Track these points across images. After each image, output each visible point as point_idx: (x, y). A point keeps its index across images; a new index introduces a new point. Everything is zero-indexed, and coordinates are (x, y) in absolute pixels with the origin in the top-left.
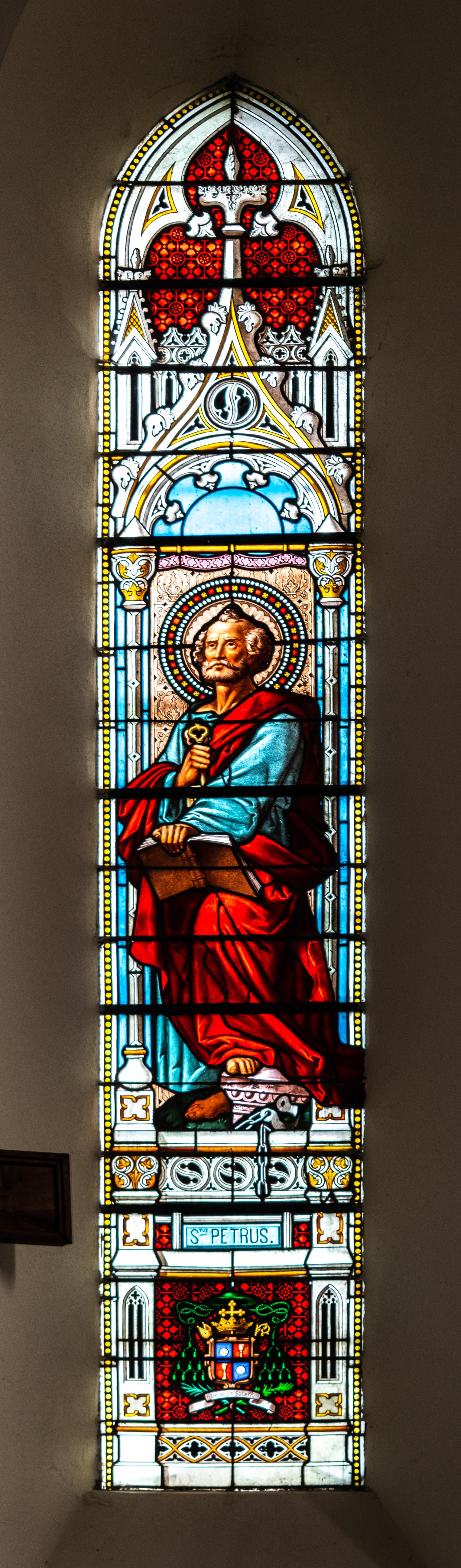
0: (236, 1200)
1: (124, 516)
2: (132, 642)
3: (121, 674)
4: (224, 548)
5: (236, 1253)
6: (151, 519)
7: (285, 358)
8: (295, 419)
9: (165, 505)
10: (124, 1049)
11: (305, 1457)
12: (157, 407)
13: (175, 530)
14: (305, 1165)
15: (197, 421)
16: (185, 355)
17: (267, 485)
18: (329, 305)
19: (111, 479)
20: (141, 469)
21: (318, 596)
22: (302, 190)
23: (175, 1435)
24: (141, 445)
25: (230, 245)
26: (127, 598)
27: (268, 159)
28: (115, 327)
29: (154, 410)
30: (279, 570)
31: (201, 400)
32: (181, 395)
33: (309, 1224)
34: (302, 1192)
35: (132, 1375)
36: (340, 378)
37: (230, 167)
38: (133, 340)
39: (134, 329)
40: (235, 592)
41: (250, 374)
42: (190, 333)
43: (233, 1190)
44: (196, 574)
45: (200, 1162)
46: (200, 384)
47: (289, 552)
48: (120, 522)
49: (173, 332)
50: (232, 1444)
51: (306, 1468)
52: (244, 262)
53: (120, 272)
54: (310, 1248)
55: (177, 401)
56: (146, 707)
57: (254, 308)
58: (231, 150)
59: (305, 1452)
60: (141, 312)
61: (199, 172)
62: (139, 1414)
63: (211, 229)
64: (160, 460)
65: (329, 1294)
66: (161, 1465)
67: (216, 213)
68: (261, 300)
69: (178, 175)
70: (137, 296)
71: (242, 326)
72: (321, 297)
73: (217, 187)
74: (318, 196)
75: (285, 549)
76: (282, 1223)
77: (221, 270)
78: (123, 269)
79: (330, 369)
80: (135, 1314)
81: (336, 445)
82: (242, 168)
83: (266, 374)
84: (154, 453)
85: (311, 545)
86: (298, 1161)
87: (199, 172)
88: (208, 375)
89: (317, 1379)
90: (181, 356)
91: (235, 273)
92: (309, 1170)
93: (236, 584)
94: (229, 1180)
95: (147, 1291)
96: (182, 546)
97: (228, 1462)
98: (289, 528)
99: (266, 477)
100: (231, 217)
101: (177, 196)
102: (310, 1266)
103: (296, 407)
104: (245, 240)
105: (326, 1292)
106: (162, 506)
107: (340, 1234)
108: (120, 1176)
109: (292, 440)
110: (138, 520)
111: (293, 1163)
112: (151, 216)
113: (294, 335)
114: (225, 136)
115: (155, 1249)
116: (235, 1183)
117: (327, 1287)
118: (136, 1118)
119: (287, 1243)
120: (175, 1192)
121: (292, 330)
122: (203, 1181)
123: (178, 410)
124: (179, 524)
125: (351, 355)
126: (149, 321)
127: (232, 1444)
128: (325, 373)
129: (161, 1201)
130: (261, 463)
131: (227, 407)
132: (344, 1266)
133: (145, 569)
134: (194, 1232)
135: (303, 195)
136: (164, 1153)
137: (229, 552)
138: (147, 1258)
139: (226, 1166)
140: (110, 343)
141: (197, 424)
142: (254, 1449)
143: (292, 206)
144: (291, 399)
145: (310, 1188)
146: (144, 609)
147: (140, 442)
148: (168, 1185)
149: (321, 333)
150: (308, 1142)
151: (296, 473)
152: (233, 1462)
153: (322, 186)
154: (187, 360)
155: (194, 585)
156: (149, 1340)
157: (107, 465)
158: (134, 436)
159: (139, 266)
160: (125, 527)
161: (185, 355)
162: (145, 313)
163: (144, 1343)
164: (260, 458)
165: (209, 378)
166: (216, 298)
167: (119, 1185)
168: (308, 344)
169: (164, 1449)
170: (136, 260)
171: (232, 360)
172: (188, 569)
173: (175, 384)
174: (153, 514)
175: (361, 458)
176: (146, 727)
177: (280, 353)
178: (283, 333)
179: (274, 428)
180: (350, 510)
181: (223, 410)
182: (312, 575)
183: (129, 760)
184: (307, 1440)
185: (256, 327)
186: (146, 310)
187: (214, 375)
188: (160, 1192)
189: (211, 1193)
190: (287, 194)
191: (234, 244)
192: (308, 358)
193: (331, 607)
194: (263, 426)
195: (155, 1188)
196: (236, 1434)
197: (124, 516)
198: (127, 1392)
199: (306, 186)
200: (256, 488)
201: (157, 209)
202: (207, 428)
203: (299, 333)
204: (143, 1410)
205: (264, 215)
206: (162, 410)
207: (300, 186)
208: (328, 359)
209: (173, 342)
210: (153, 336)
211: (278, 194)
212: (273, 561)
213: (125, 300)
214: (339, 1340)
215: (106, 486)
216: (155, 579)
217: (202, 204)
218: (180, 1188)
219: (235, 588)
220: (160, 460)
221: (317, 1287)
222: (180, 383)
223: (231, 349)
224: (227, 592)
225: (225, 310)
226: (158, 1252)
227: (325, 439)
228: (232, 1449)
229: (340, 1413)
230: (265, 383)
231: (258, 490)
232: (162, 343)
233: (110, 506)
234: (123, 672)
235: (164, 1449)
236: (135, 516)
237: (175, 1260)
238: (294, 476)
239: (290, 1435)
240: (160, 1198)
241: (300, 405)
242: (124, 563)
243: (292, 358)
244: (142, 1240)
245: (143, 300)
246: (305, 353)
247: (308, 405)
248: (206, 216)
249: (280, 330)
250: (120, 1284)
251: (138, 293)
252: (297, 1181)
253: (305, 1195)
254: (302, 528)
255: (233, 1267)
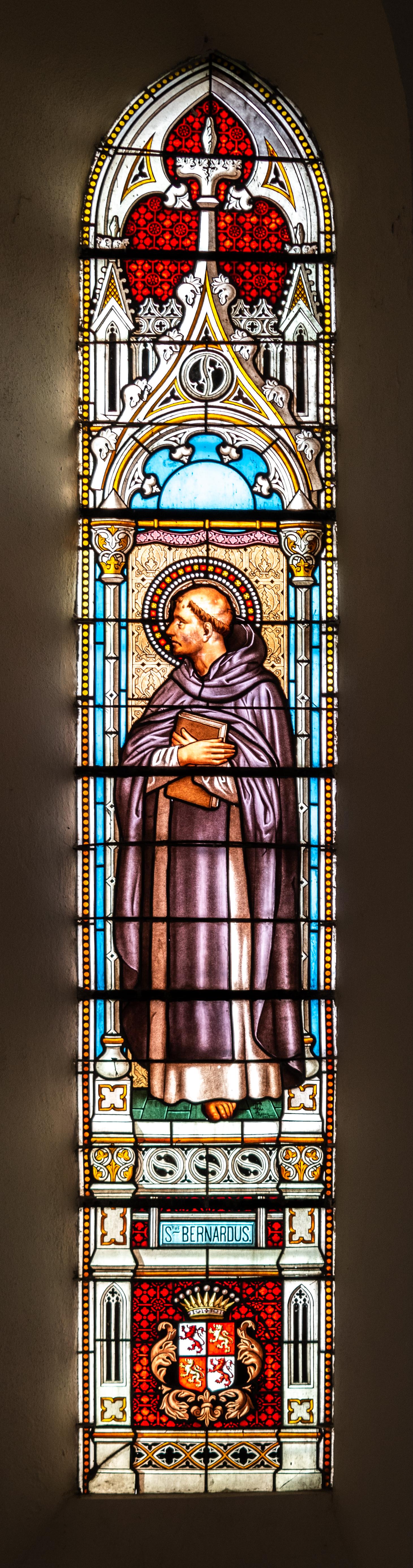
0: (210, 1193)
1: (103, 488)
2: (110, 614)
3: (100, 648)
4: (200, 524)
5: (211, 1251)
6: (128, 492)
7: (256, 332)
8: (267, 392)
9: (142, 477)
10: (102, 1037)
11: (278, 1464)
12: (134, 377)
13: (151, 504)
14: (277, 1157)
15: (173, 392)
16: (161, 326)
17: (240, 458)
18: (299, 280)
19: (91, 451)
20: (119, 439)
21: (290, 576)
22: (275, 166)
23: (150, 1441)
24: (119, 417)
25: (205, 217)
26: (106, 570)
27: (244, 134)
28: (94, 296)
29: (131, 381)
30: (253, 548)
31: (176, 372)
32: (157, 366)
33: (282, 1222)
34: (274, 1185)
35: (109, 1378)
36: (310, 353)
37: (207, 139)
38: (111, 309)
39: (113, 299)
40: (211, 573)
41: (224, 347)
42: (166, 303)
43: (207, 1183)
44: (173, 549)
45: (174, 1153)
46: (176, 355)
47: (262, 530)
48: (99, 494)
49: (150, 303)
50: (206, 1450)
51: (278, 1476)
52: (218, 233)
53: (98, 239)
54: (283, 1247)
55: (154, 372)
56: (123, 687)
57: (227, 281)
58: (209, 122)
59: (276, 1459)
60: (119, 283)
61: (177, 143)
62: (116, 1419)
63: (188, 200)
64: (138, 431)
65: (300, 1294)
66: (137, 1474)
67: (192, 183)
68: (234, 273)
69: (157, 145)
70: (115, 265)
71: (216, 298)
72: (291, 272)
73: (194, 159)
74: (292, 173)
75: (258, 527)
76: (256, 1221)
77: (197, 242)
78: (103, 237)
79: (300, 344)
80: (112, 1311)
81: (304, 419)
82: (219, 141)
83: (238, 347)
84: (131, 424)
85: (282, 522)
86: (271, 1153)
87: (177, 143)
88: (184, 346)
89: (290, 1384)
90: (157, 326)
91: (209, 247)
92: (281, 1161)
93: (213, 565)
94: (204, 1172)
95: (125, 1289)
96: (159, 520)
97: (201, 1469)
98: (261, 503)
99: (239, 450)
100: (207, 188)
101: (156, 165)
102: (283, 1266)
103: (268, 381)
104: (218, 211)
105: (298, 1292)
106: (139, 478)
107: (313, 1234)
108: (98, 1168)
109: (263, 414)
110: (117, 493)
111: (266, 1154)
112: (130, 184)
113: (266, 309)
114: (203, 107)
115: (132, 1248)
116: (210, 1175)
117: (299, 1287)
118: (115, 1108)
119: (262, 1242)
120: (152, 1184)
121: (263, 304)
122: (178, 1174)
123: (154, 382)
124: (156, 498)
125: (320, 329)
126: (127, 291)
127: (206, 1450)
128: (295, 347)
129: (137, 1193)
130: (234, 436)
131: (202, 380)
132: (316, 1266)
133: (123, 542)
134: (168, 1229)
135: (276, 173)
136: (139, 1145)
137: (204, 528)
138: (124, 1258)
139: (201, 1158)
140: (89, 312)
141: (173, 396)
142: (227, 1455)
143: (265, 182)
144: (262, 372)
145: (282, 1180)
146: (122, 582)
147: (118, 413)
148: (144, 1177)
149: (291, 307)
150: (280, 1132)
151: (268, 448)
152: (206, 1469)
153: (294, 164)
154: (163, 331)
155: (172, 562)
156: (126, 1340)
157: (86, 436)
158: (112, 407)
159: (117, 234)
160: (103, 500)
161: (161, 326)
162: (123, 284)
163: (121, 1343)
164: (233, 432)
165: (185, 349)
166: (192, 271)
167: (97, 1177)
168: (279, 318)
169: (141, 1455)
170: (115, 227)
171: (207, 332)
172: (165, 544)
173: (152, 354)
174: (130, 487)
175: (330, 436)
176: (123, 710)
177: (253, 327)
178: (255, 307)
179: (246, 401)
180: (320, 487)
181: (198, 383)
182: (285, 554)
183: (106, 699)
184: (278, 1447)
185: (229, 299)
186: (124, 280)
187: (189, 347)
188: (136, 1185)
189: (186, 1185)
190: (261, 169)
191: (210, 216)
192: (279, 331)
193: (302, 587)
194: (236, 399)
195: (132, 1181)
196: (210, 1440)
197: (103, 488)
198: (103, 1396)
199: (280, 164)
200: (229, 462)
201: (136, 178)
202: (182, 400)
203: (270, 307)
204: (120, 1416)
205: (238, 189)
206: (139, 381)
207: (274, 163)
208: (299, 334)
209: (149, 313)
210: (131, 306)
211: (252, 169)
212: (246, 539)
213: (104, 270)
214: (310, 1342)
215: (86, 458)
216: (134, 552)
217: (180, 175)
218: (156, 1180)
219: (211, 569)
220: (138, 431)
221: (289, 1287)
222: (157, 355)
223: (205, 321)
224: (203, 572)
225: (200, 282)
226: (135, 1251)
227: (295, 414)
228: (206, 1455)
229: (311, 1421)
230: (238, 355)
231: (232, 464)
232: (140, 314)
233: (90, 478)
234: (102, 646)
235: (141, 1455)
236: (113, 489)
237: (151, 1259)
238: (265, 450)
239: (263, 1441)
240: (136, 1191)
241: (272, 379)
242: (104, 535)
243: (264, 332)
244: (120, 1239)
245: (121, 270)
246: (276, 327)
247: (278, 378)
248: (183, 189)
249: (252, 303)
250: (99, 1284)
251: (116, 263)
252: (270, 1173)
253: (277, 1188)
254: (274, 503)
255: (207, 1265)
